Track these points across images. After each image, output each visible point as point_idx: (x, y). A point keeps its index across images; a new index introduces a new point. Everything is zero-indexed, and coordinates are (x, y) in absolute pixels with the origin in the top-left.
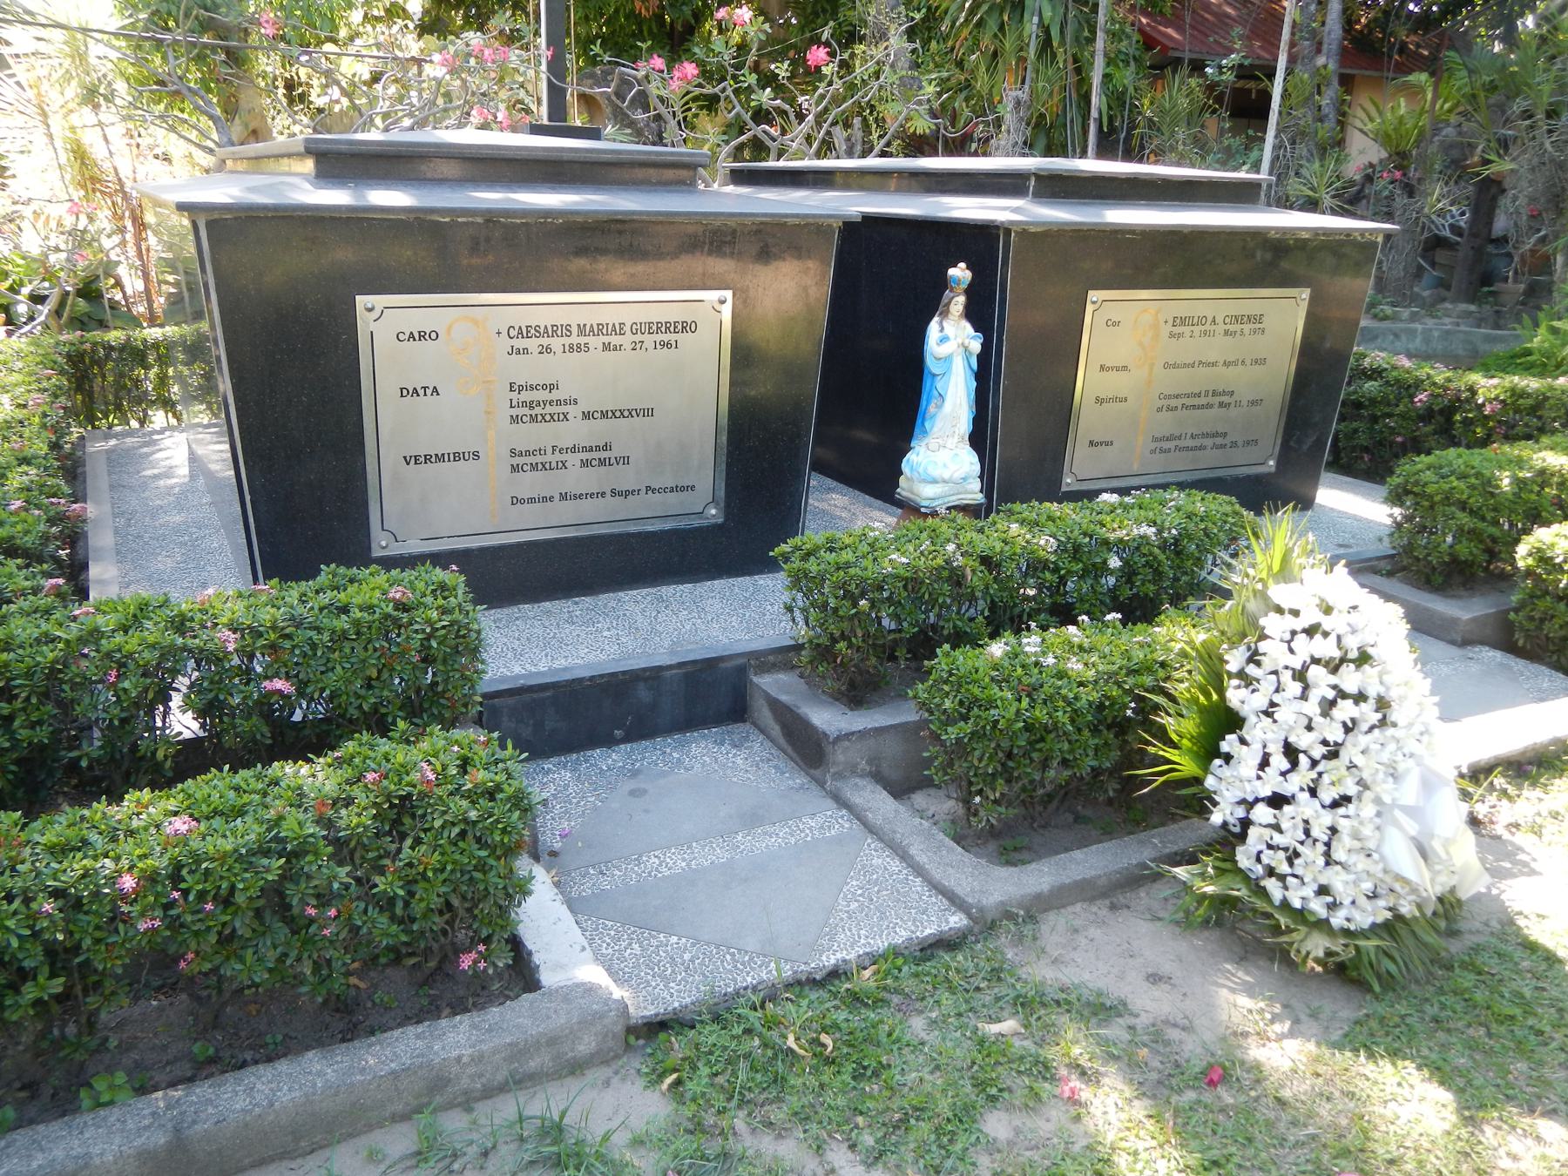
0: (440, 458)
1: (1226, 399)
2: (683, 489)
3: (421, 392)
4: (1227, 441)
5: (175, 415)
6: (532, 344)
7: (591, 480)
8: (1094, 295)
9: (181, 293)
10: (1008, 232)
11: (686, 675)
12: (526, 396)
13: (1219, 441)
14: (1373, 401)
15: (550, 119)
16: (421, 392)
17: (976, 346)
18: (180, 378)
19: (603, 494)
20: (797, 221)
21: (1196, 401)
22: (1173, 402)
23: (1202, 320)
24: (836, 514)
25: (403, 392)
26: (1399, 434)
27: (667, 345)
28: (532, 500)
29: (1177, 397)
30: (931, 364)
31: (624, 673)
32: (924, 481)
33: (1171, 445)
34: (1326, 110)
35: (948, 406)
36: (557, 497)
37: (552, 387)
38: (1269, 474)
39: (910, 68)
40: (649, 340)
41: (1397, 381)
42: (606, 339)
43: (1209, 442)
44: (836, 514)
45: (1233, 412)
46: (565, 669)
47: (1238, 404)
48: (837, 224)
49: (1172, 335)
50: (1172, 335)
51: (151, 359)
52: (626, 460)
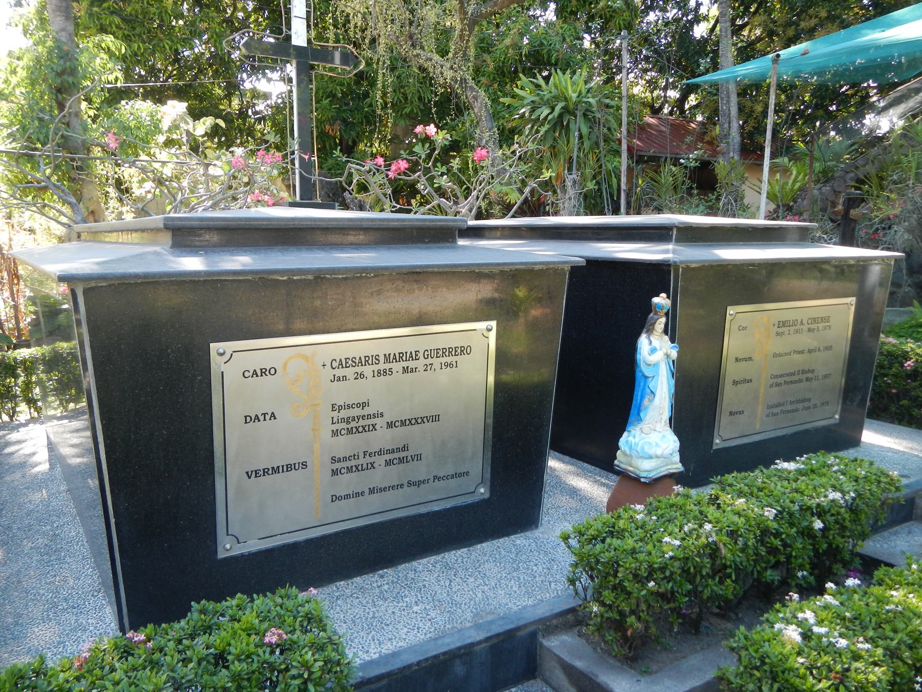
0: (276, 470)
1: (809, 375)
2: (460, 475)
3: (262, 418)
4: (811, 404)
5: (36, 409)
6: (350, 372)
7: (393, 475)
8: (731, 310)
9: (38, 318)
11: (492, 647)
12: (344, 414)
15: (301, 199)
16: (262, 418)
17: (674, 354)
18: (40, 383)
19: (402, 486)
20: (540, 267)
22: (779, 380)
23: (795, 322)
24: (573, 486)
25: (247, 419)
26: (894, 388)
27: (449, 365)
28: (347, 497)
29: (781, 376)
30: (643, 368)
31: (444, 654)
32: (642, 457)
36: (367, 492)
37: (364, 405)
40: (436, 362)
41: (889, 352)
42: (405, 364)
43: (800, 406)
44: (573, 486)
45: (815, 384)
46: (394, 655)
47: (817, 378)
48: (567, 268)
49: (778, 334)
50: (778, 334)
51: (19, 371)
52: (419, 457)
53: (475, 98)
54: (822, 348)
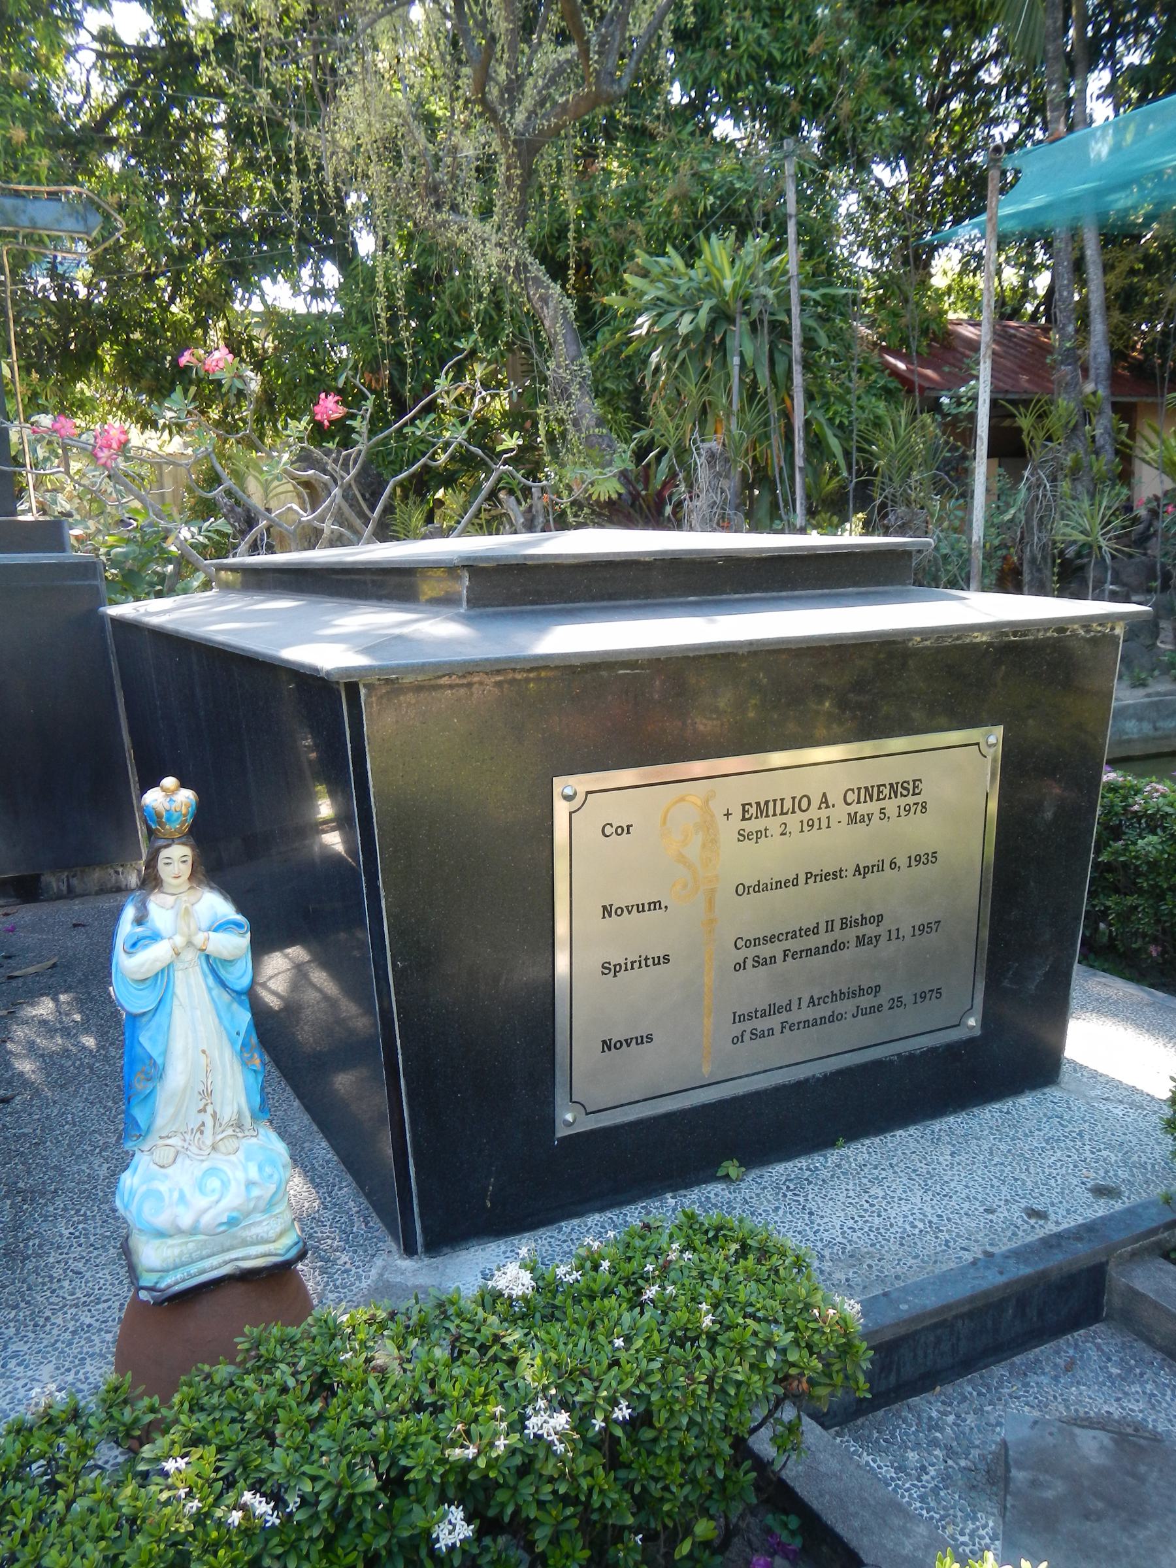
1: (869, 930)
8: (562, 785)
10: (352, 689)
13: (865, 1001)
14: (1153, 865)
21: (812, 942)
23: (799, 804)
29: (771, 939)
33: (774, 1022)
34: (1100, 442)
35: (178, 1075)
38: (971, 1041)
39: (598, 426)
45: (887, 949)
47: (894, 935)
49: (743, 836)
50: (743, 836)
53: (544, 300)
54: (902, 861)
